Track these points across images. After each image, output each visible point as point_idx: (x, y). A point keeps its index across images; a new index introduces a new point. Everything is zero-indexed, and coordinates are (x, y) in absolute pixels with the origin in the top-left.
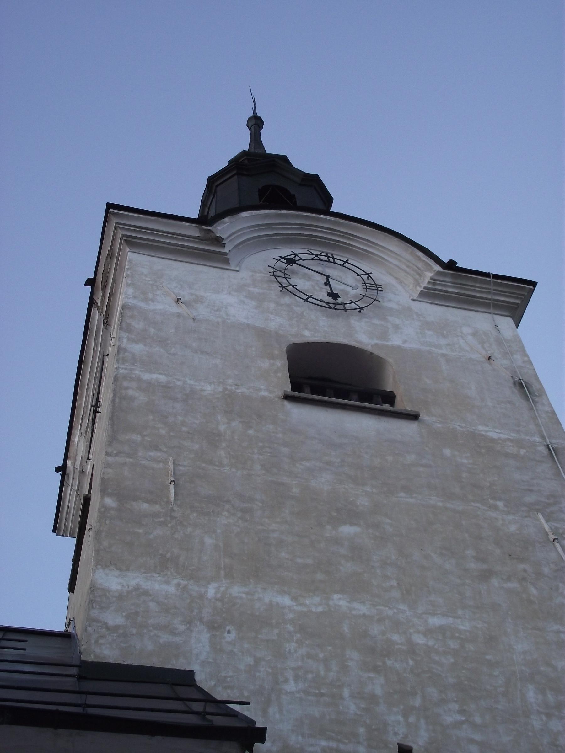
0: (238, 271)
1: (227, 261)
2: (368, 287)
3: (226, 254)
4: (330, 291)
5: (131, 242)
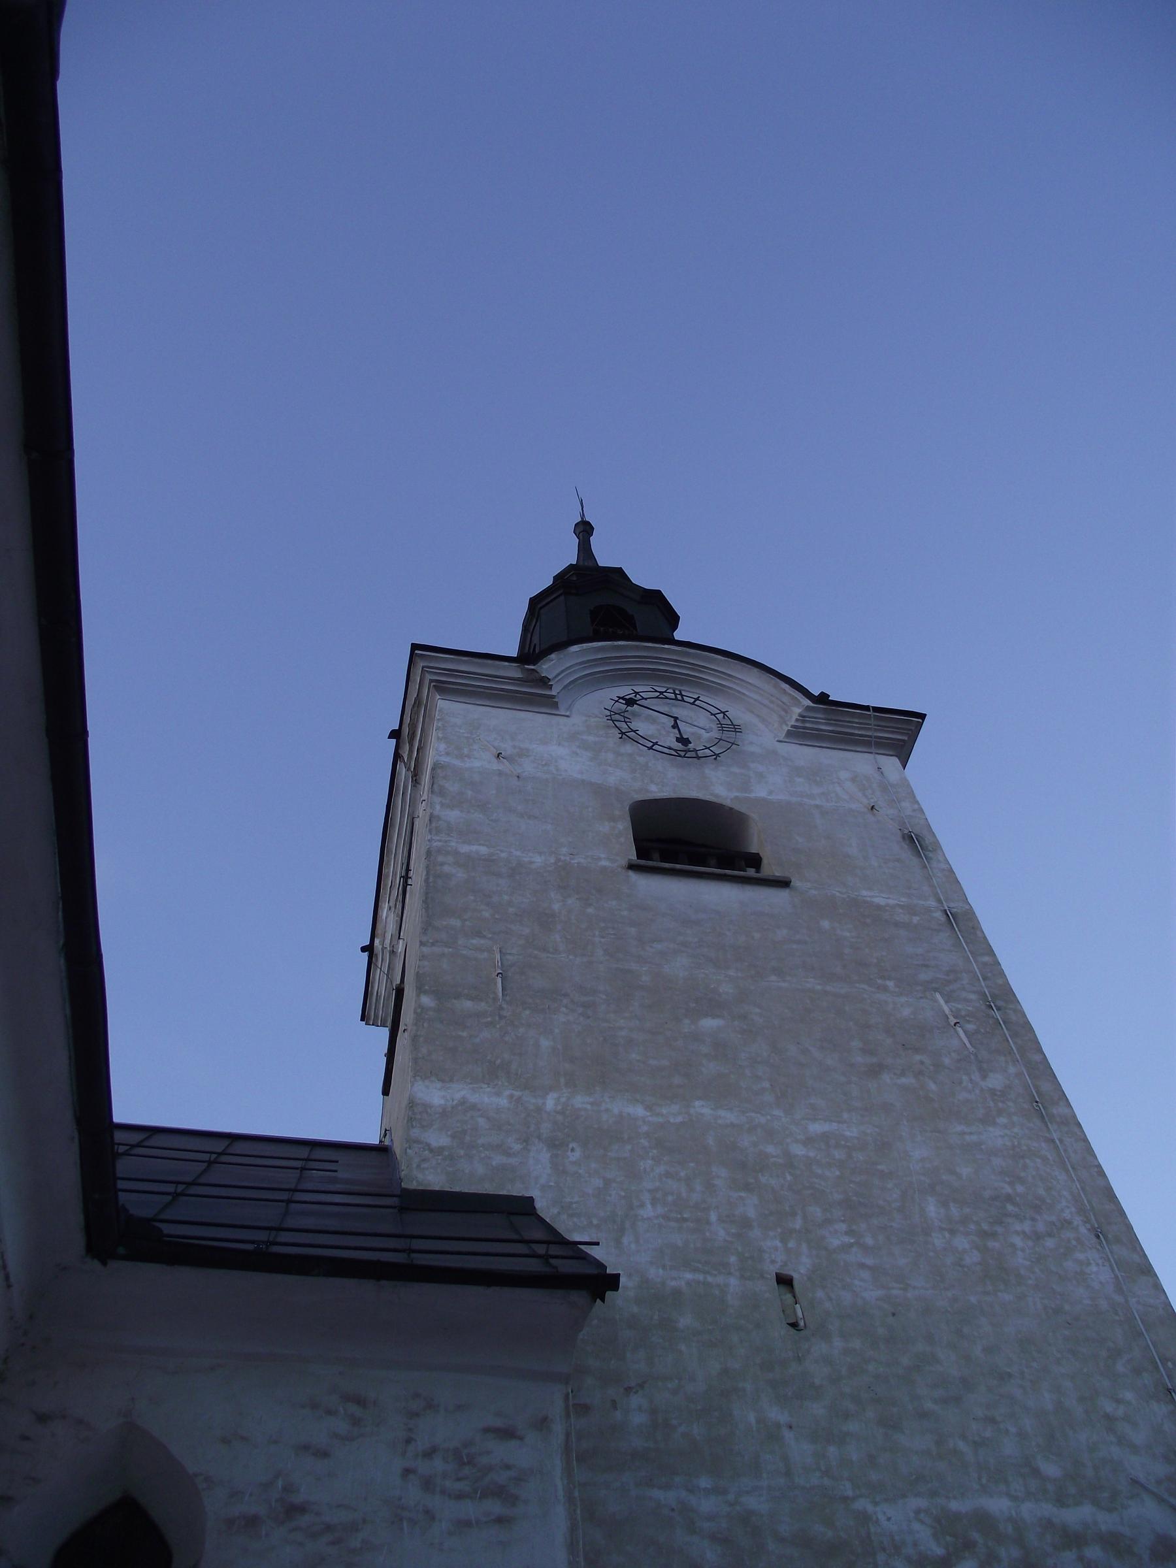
0: (568, 716)
1: (555, 705)
3: (553, 697)
4: (678, 736)
5: (441, 688)
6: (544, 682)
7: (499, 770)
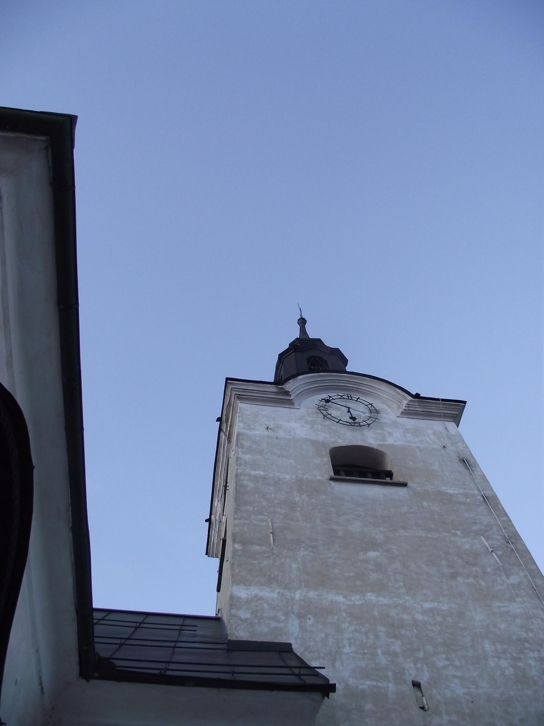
0: (298, 409)
1: (293, 404)
2: (372, 412)
3: (292, 400)
4: (351, 416)
5: (240, 397)
6: (287, 393)
7: (268, 435)
